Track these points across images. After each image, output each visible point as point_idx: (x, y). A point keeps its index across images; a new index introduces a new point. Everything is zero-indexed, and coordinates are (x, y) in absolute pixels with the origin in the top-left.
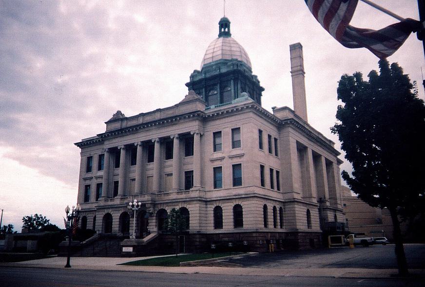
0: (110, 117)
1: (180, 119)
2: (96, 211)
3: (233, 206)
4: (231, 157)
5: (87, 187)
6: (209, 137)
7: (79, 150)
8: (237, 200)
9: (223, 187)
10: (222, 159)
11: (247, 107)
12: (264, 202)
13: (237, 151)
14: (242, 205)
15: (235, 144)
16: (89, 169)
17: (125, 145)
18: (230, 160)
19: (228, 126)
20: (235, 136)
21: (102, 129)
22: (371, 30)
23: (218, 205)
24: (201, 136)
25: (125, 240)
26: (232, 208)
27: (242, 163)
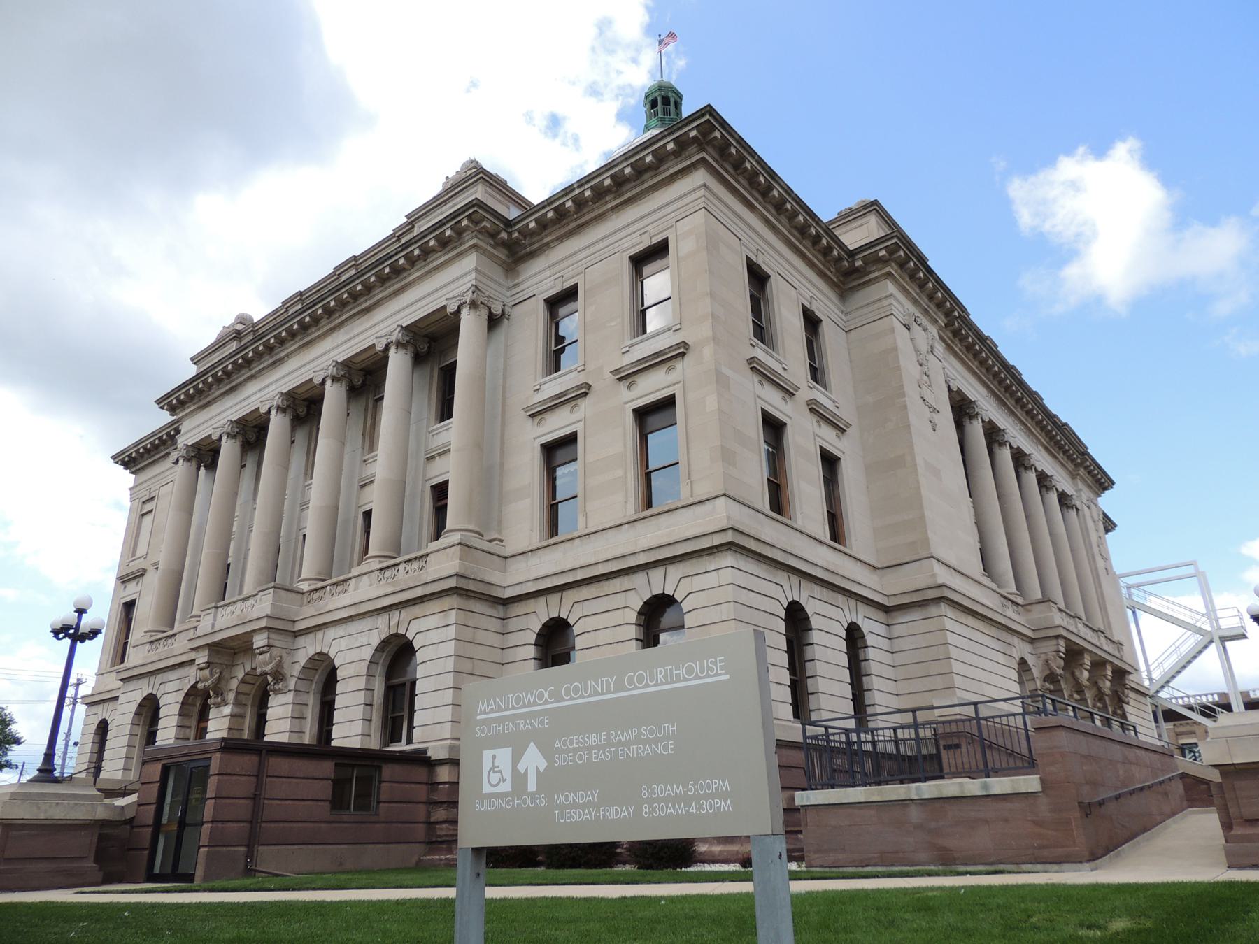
5: (129, 606)
6: (528, 327)
24: (494, 322)
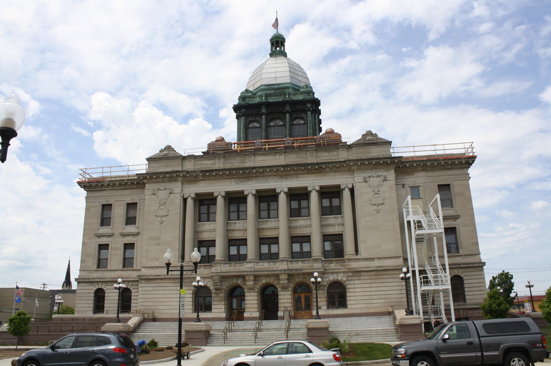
0: (154, 151)
1: (157, 178)
2: (138, 281)
3: (95, 289)
4: (123, 235)
7: (83, 193)
8: (100, 284)
9: (135, 266)
10: (111, 235)
11: (120, 184)
12: (359, 257)
13: (131, 229)
14: (104, 289)
15: (130, 220)
16: (105, 221)
17: (195, 194)
18: (97, 238)
19: (123, 199)
20: (105, 212)
21: (142, 168)
22: (384, 139)
23: (102, 288)
25: (107, 324)
26: (94, 292)
27: (110, 243)
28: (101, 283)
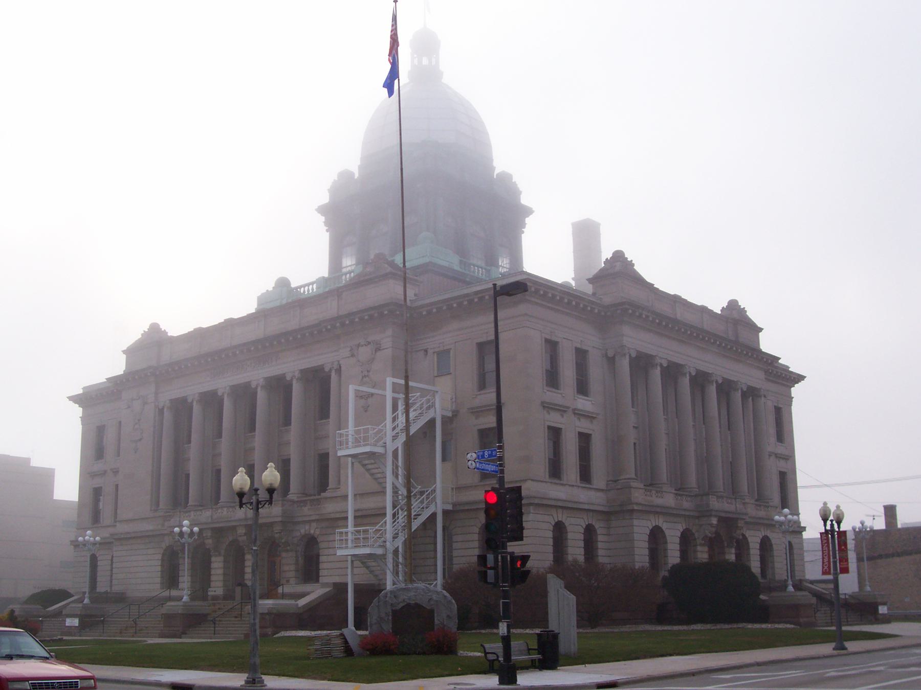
28: (560, 511)
